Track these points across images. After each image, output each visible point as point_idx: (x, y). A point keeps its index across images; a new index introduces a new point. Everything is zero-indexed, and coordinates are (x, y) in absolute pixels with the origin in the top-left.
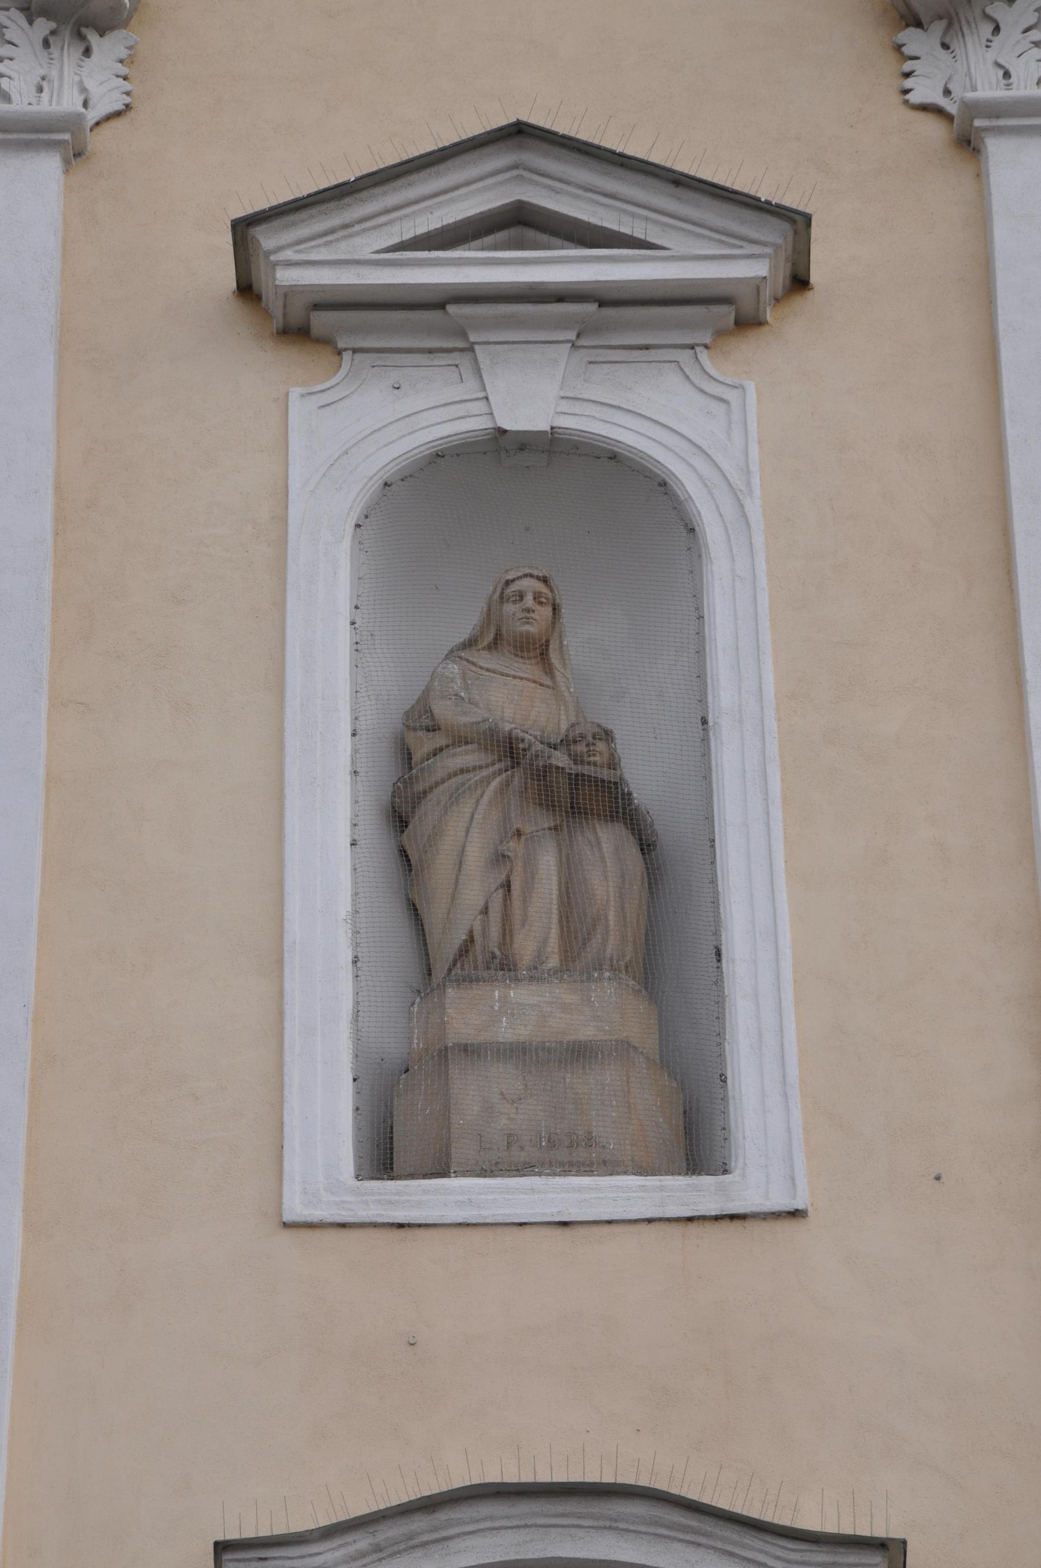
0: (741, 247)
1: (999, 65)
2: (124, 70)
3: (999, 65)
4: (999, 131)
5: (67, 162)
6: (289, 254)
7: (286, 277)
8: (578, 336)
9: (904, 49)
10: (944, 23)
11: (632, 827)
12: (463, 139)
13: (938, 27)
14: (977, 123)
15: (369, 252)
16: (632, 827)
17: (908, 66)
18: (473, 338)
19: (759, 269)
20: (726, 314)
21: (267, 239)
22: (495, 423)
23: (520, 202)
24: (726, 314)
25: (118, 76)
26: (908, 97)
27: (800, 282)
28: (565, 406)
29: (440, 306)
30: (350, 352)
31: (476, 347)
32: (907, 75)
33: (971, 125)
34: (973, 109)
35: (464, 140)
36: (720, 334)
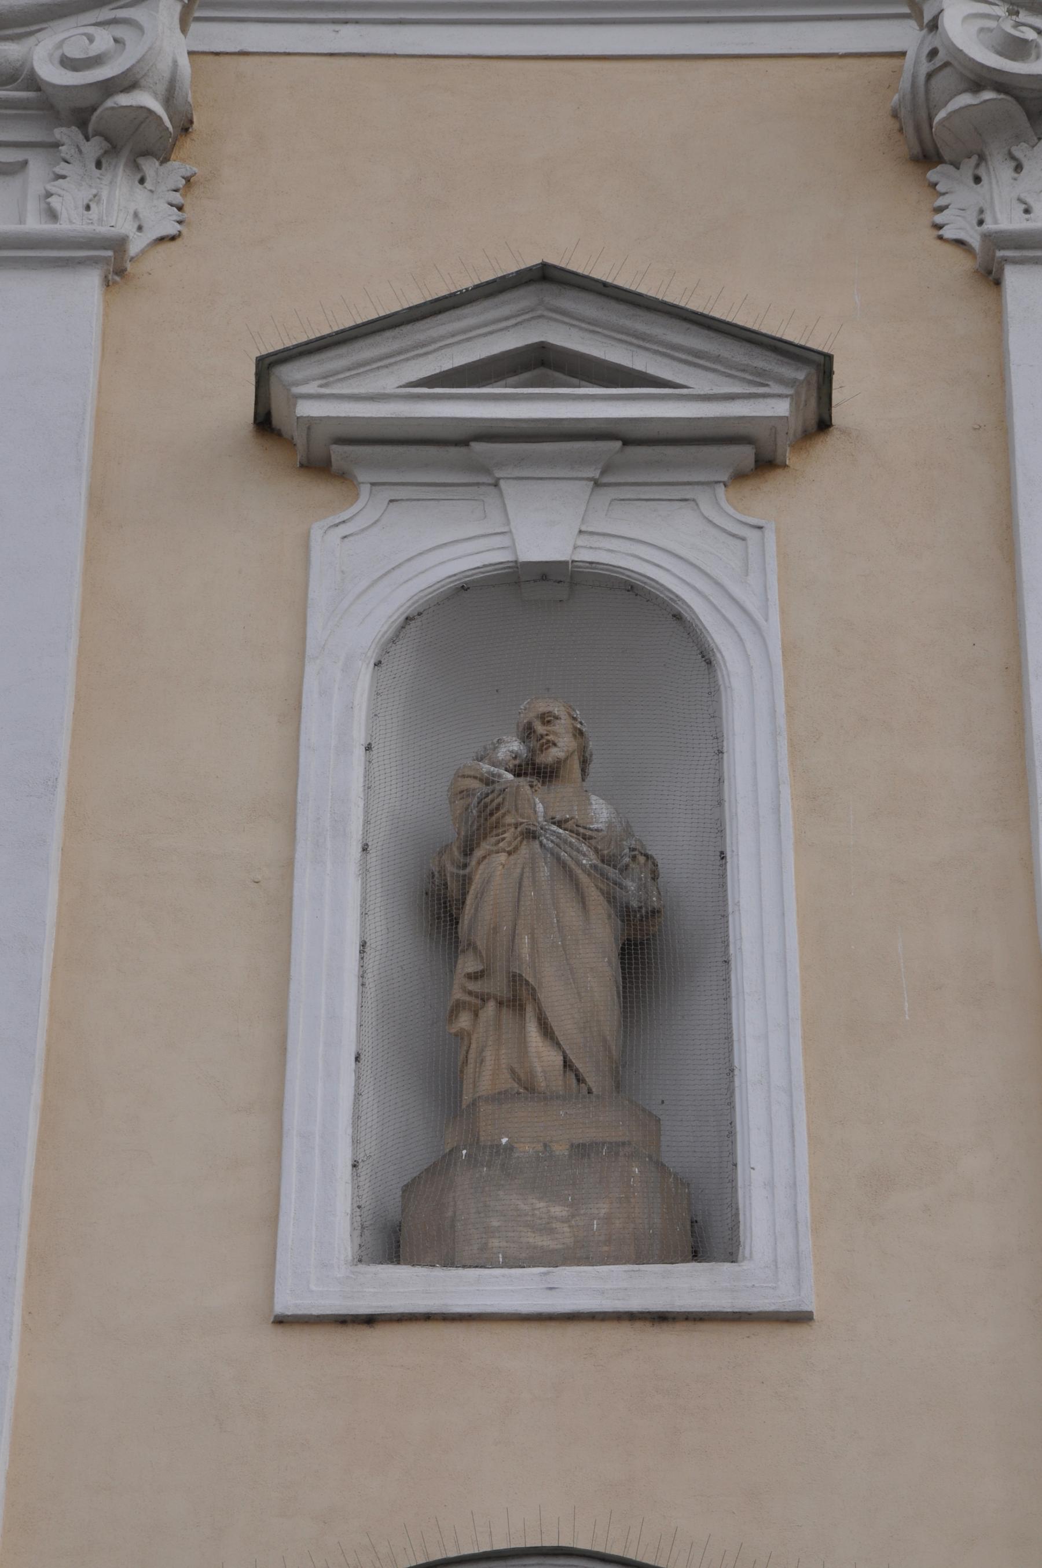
0: (767, 385)
1: (1020, 200)
2: (177, 198)
3: (1020, 200)
4: (1015, 262)
5: (107, 283)
6: (312, 388)
7: (307, 409)
8: (603, 472)
9: (938, 187)
10: (974, 159)
11: (637, 962)
12: (358, 323)
13: (970, 163)
14: (1000, 254)
15: (397, 385)
16: (637, 962)
17: (941, 202)
18: (498, 474)
19: (781, 408)
20: (745, 455)
21: (289, 372)
22: (516, 555)
23: (542, 342)
24: (745, 455)
25: (172, 205)
26: (941, 232)
27: (824, 425)
28: (583, 541)
29: (463, 442)
30: (369, 485)
31: (502, 483)
32: (940, 210)
33: (994, 256)
34: (996, 241)
35: (359, 324)
36: (740, 476)
